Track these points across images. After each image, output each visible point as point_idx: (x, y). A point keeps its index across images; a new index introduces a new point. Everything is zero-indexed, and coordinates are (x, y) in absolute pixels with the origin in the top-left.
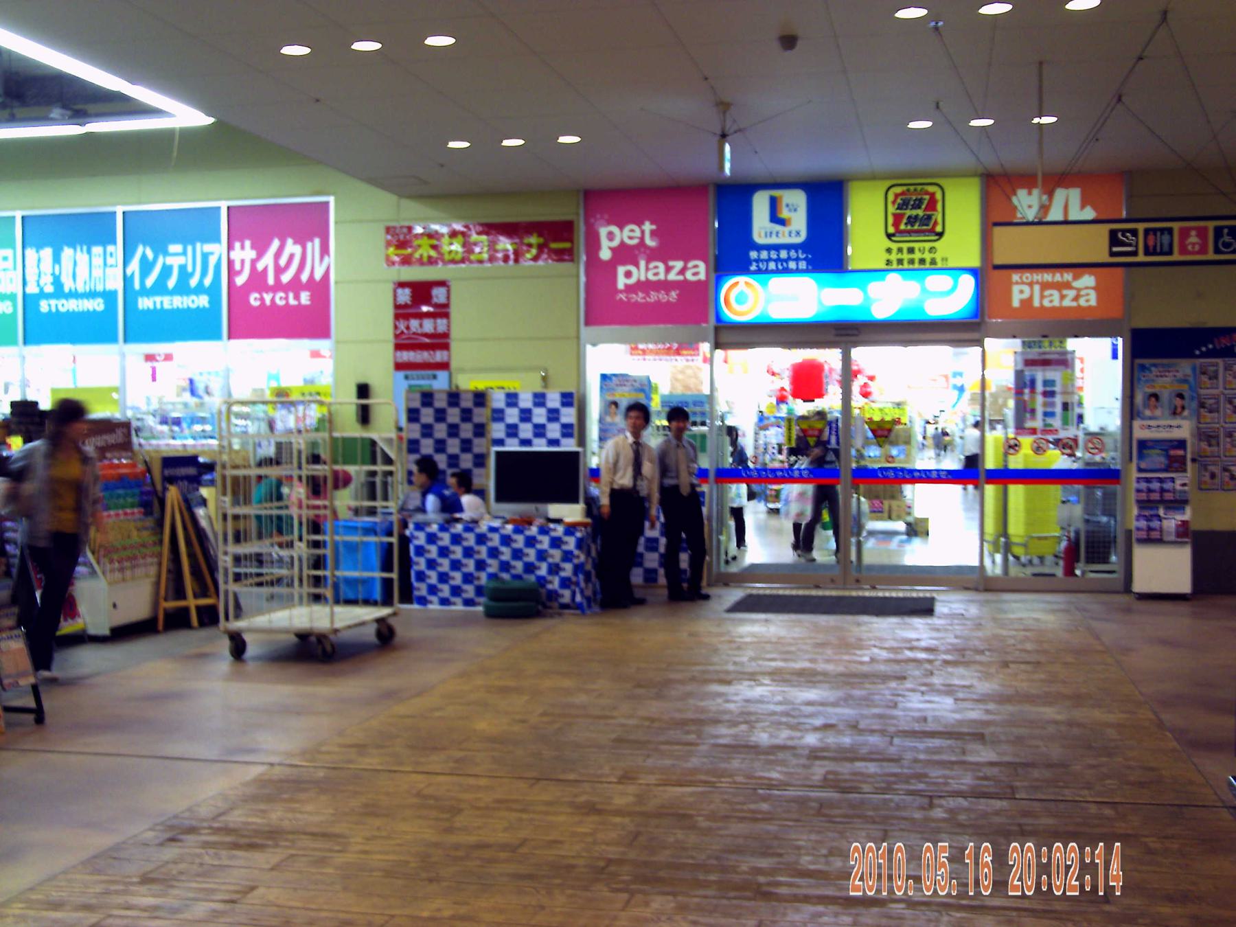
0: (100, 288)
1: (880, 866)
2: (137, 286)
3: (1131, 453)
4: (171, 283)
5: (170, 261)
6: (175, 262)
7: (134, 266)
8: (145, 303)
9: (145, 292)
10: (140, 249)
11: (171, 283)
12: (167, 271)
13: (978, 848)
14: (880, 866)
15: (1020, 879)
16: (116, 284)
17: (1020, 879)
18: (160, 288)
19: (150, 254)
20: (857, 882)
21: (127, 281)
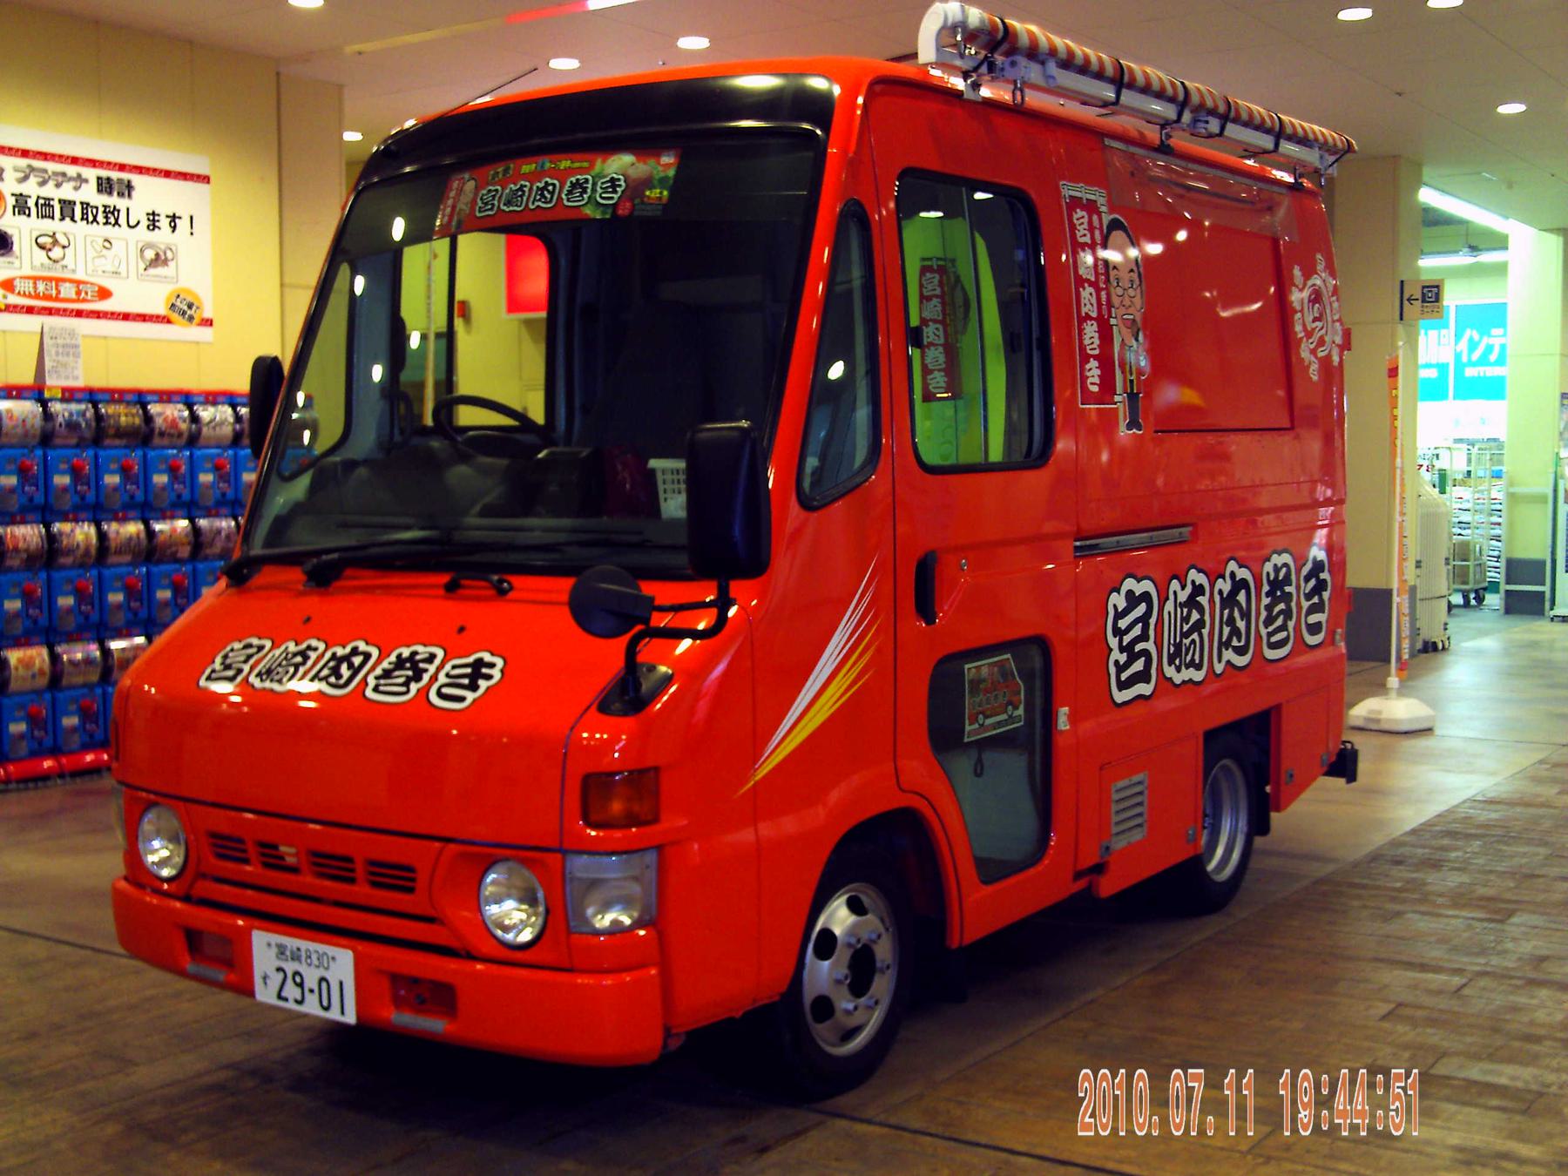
0: (1434, 361)
1: (1116, 1097)
2: (1465, 359)
3: (473, 844)
4: (1493, 358)
5: (1491, 341)
6: (1497, 342)
7: (1463, 345)
8: (1470, 372)
9: (1471, 364)
10: (1468, 332)
11: (1493, 358)
12: (1490, 348)
13: (1294, 1076)
14: (1116, 1097)
15: (1093, 1115)
16: (1450, 360)
17: (1093, 1115)
18: (1483, 361)
19: (1476, 338)
20: (1087, 1120)
21: (1458, 356)
